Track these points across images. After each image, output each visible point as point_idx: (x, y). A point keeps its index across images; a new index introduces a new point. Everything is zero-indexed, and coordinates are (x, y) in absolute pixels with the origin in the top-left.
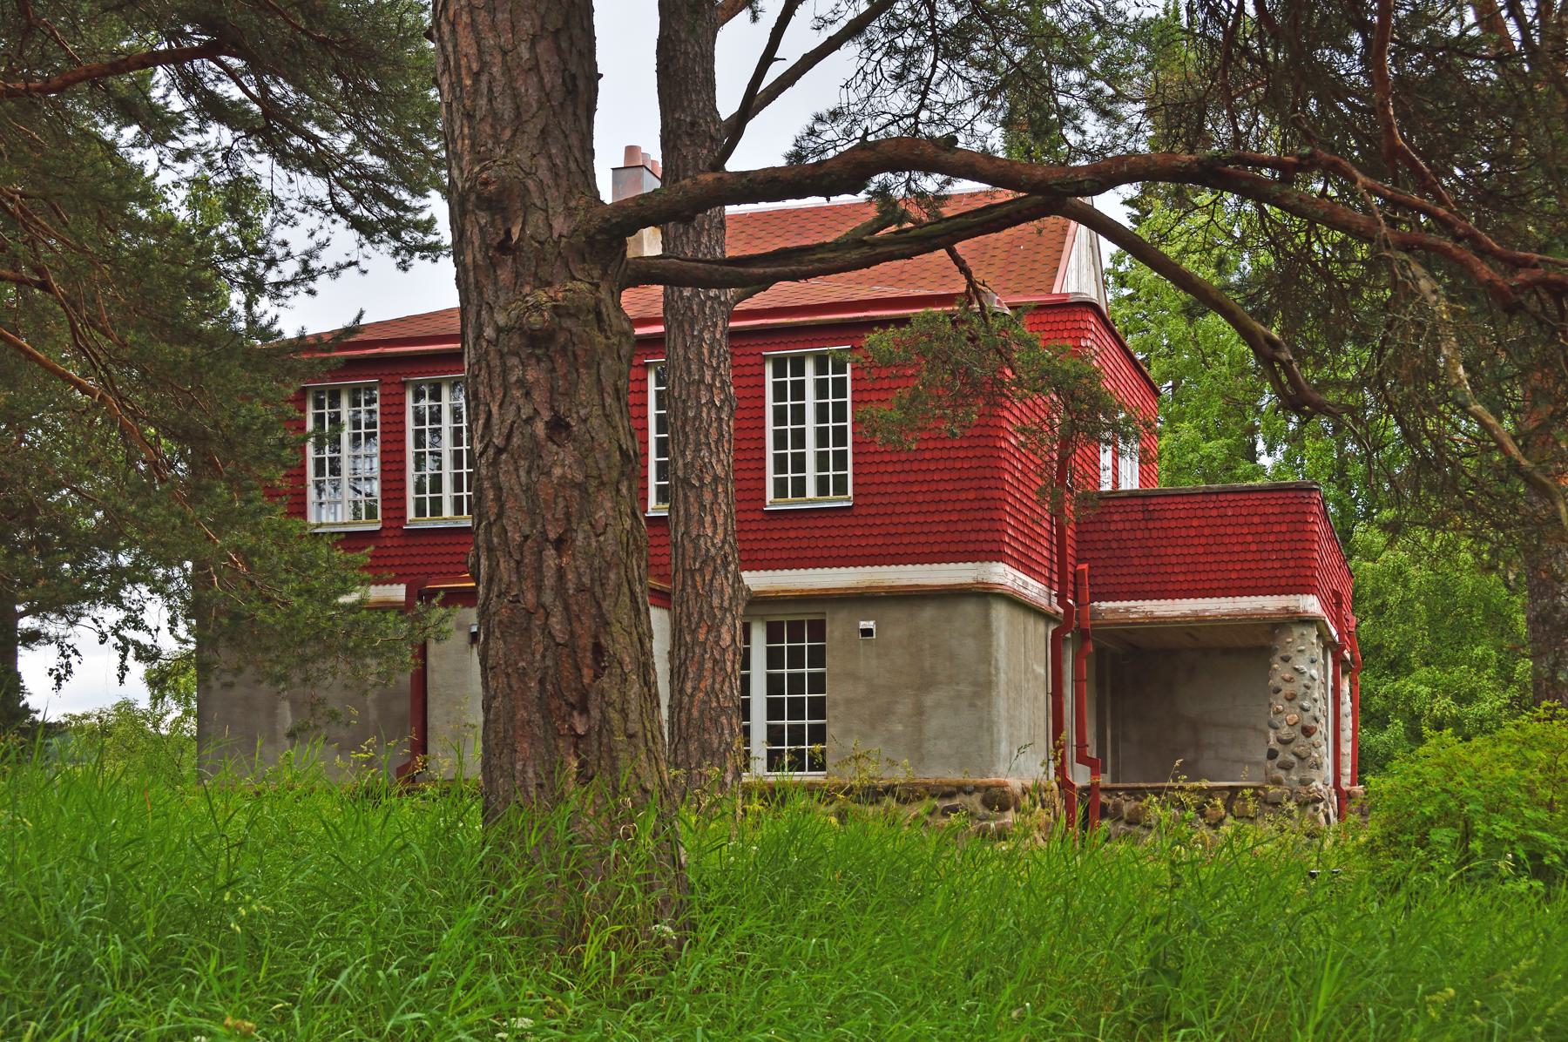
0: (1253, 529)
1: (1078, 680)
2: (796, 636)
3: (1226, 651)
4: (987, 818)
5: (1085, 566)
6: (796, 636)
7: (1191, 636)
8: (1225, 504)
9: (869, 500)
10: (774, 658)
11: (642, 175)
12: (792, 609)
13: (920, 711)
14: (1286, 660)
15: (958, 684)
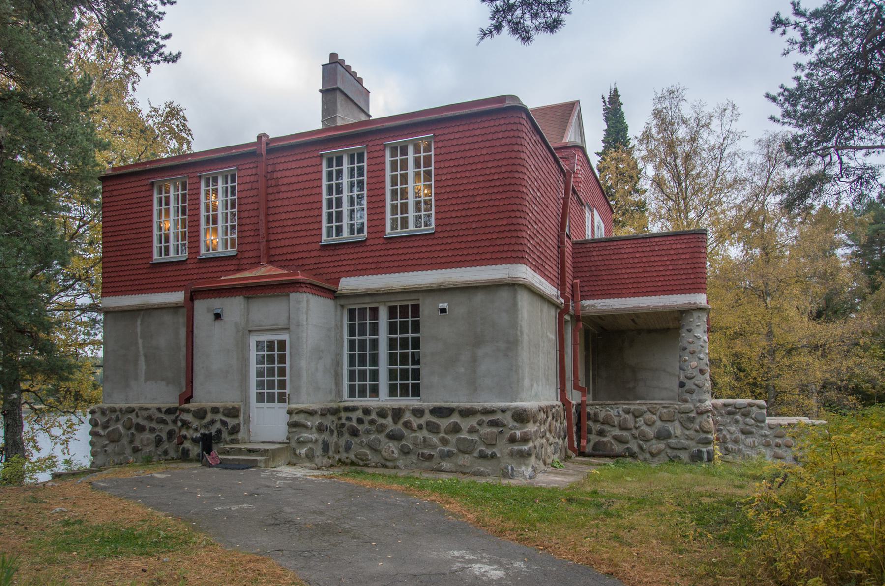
0: (670, 257)
1: (575, 344)
2: (404, 314)
3: (650, 331)
4: (515, 428)
5: (578, 281)
6: (404, 314)
7: (633, 320)
8: (654, 244)
9: (444, 228)
10: (392, 329)
11: (336, 66)
12: (400, 297)
13: (474, 360)
14: (689, 331)
15: (497, 342)
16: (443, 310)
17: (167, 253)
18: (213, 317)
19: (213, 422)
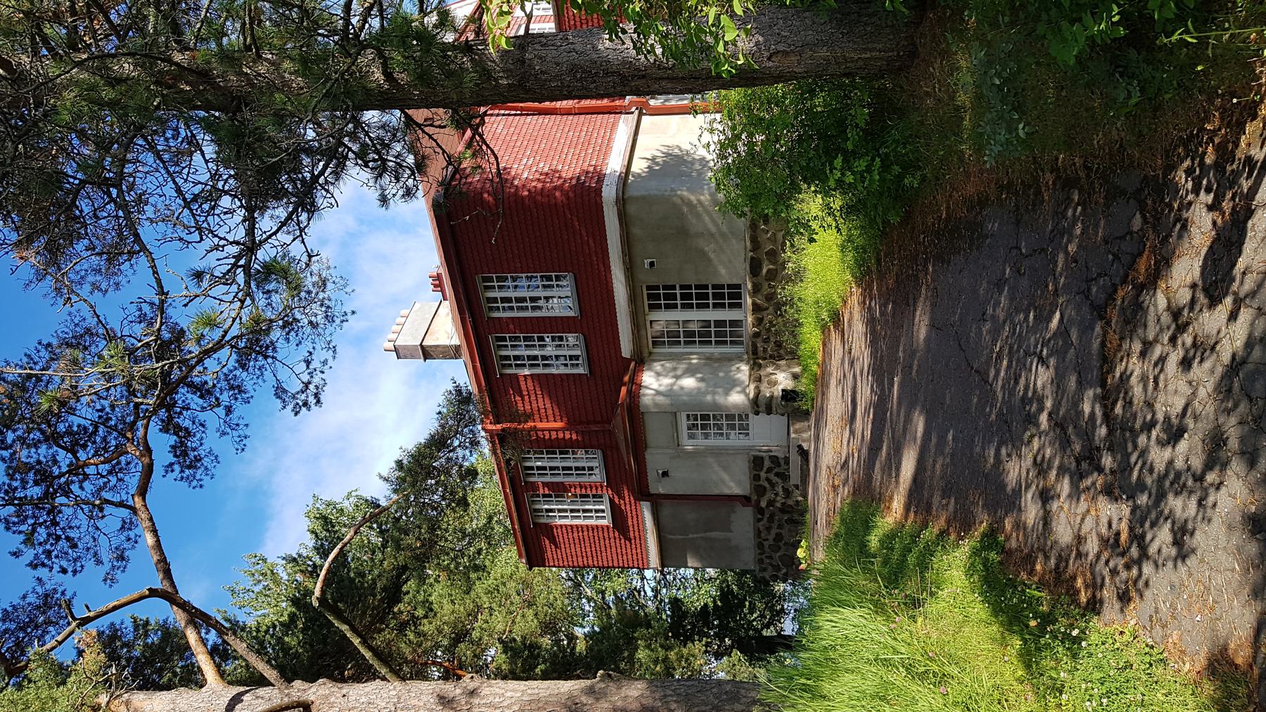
2: (657, 297)
6: (657, 297)
16: (652, 264)
17: (577, 358)
18: (666, 478)
19: (768, 479)
